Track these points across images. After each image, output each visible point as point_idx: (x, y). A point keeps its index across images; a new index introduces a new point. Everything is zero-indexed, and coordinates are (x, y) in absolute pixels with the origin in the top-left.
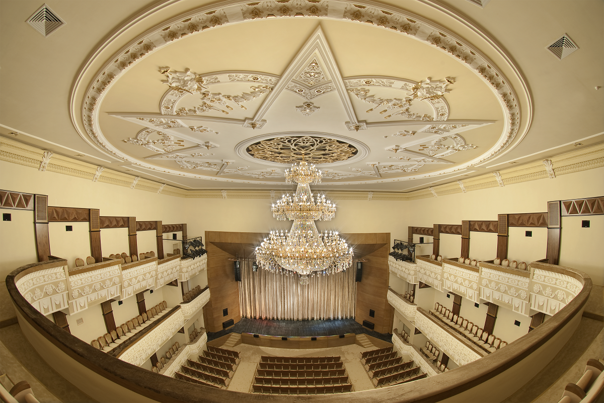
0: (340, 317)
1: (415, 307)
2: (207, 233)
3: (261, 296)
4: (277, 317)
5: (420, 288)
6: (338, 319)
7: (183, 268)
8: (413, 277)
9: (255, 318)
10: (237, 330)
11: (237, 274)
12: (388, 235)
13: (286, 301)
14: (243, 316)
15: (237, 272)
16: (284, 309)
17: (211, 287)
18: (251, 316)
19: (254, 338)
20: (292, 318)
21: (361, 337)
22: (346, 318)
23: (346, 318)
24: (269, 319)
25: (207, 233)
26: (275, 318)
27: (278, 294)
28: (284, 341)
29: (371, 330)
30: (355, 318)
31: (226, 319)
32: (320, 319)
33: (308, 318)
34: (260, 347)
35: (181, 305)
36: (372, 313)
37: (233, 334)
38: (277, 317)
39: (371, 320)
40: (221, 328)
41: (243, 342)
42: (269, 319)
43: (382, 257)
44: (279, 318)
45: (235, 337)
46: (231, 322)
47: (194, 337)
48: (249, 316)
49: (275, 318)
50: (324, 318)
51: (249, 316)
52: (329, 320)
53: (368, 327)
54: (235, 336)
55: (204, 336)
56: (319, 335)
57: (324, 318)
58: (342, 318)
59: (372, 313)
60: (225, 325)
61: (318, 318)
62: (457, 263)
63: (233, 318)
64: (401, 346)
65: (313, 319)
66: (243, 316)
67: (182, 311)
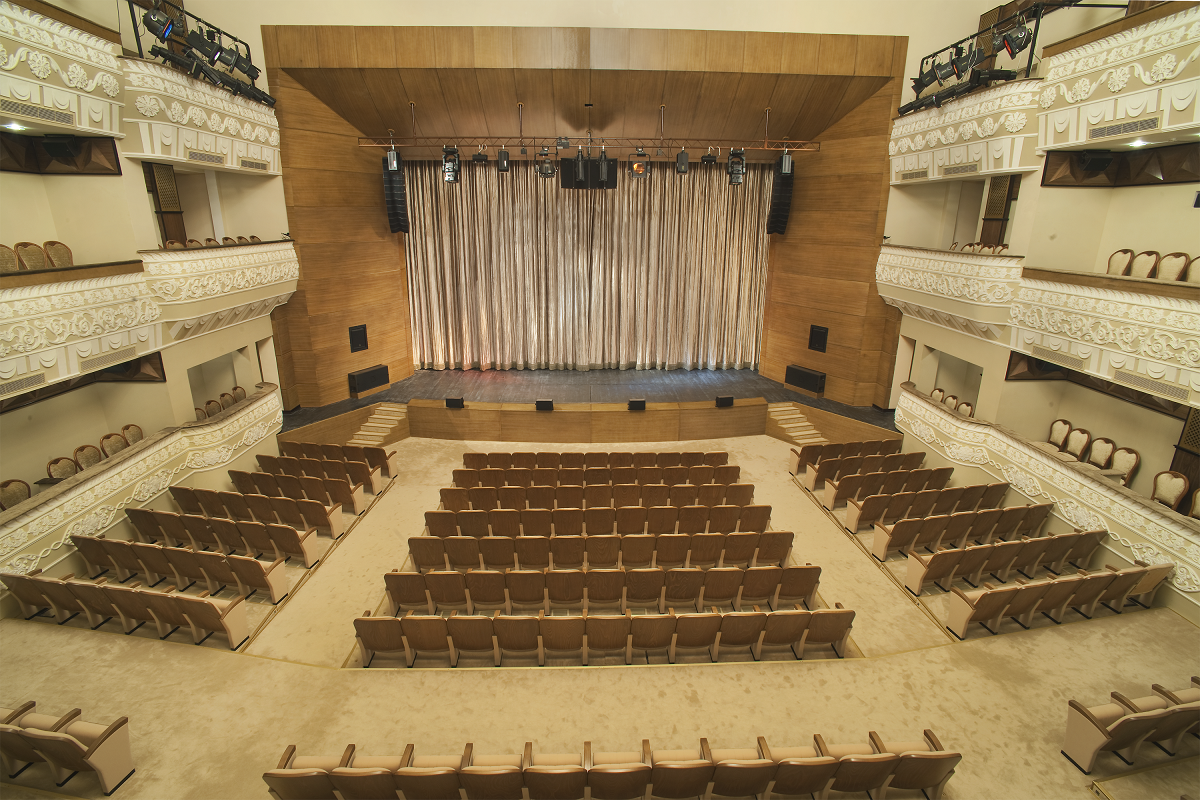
0: (712, 363)
1: (1015, 268)
2: (270, 34)
3: (476, 293)
4: (526, 363)
5: (1044, 184)
6: (705, 368)
7: (142, 93)
8: (1020, 140)
9: (459, 368)
10: (396, 395)
11: (393, 202)
12: (900, 44)
13: (552, 306)
14: (423, 364)
15: (392, 195)
16: (547, 335)
17: (300, 241)
18: (447, 364)
19: (450, 413)
20: (570, 361)
21: (783, 412)
22: (731, 368)
23: (731, 368)
24: (502, 370)
25: (270, 34)
26: (521, 362)
27: (529, 282)
28: (543, 416)
29: (814, 395)
30: (756, 369)
31: (363, 362)
32: (653, 367)
33: (618, 363)
34: (467, 442)
35: (146, 259)
36: (818, 339)
37: (384, 407)
38: (526, 363)
39: (813, 362)
40: (344, 394)
41: (414, 433)
42: (502, 370)
43: (867, 133)
44: (532, 361)
45: (387, 415)
46: (379, 375)
47: (216, 401)
48: (440, 361)
49: (521, 362)
50: (664, 364)
51: (440, 361)
52: (679, 369)
53: (805, 384)
54: (389, 413)
55: (272, 406)
56: (654, 400)
57: (664, 364)
58: (718, 368)
59: (818, 339)
60: (358, 382)
61: (647, 362)
62: (1005, 252)
63: (384, 363)
64: (946, 431)
65: (632, 367)
66: (423, 364)
67: (150, 283)
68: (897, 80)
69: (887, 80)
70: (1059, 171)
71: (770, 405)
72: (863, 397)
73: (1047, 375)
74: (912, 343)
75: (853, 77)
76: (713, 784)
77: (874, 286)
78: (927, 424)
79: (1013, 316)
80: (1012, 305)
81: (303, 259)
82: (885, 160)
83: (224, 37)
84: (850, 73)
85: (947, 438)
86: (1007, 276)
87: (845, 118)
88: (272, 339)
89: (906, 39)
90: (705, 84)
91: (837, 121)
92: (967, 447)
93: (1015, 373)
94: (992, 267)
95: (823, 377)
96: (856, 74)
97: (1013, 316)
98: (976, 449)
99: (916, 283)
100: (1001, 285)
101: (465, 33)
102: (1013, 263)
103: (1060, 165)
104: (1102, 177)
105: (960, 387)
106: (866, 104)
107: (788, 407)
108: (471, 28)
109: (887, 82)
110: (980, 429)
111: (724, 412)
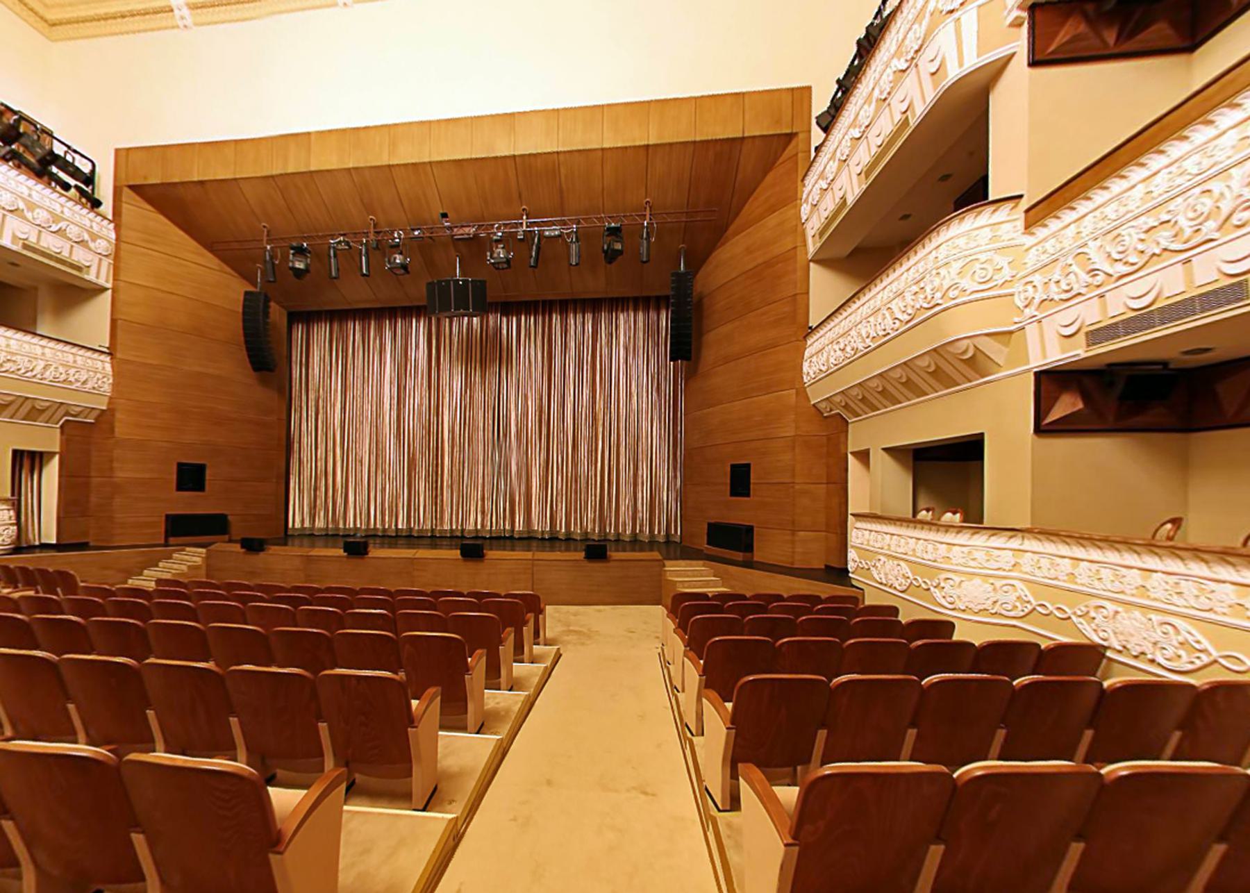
5: (1034, 63)
17: (119, 355)
29: (739, 556)
36: (740, 480)
39: (738, 512)
68: (801, 136)
69: (790, 137)
70: (1062, 33)
71: (667, 563)
72: (812, 551)
73: (1200, 38)
74: (864, 456)
75: (743, 139)
76: (1081, 846)
77: (802, 392)
78: (897, 558)
79: (1021, 305)
80: (1017, 288)
81: (116, 374)
82: (798, 228)
83: (55, 142)
84: (740, 135)
85: (931, 569)
86: (994, 238)
87: (747, 206)
88: (57, 458)
89: (808, 89)
90: (563, 171)
91: (737, 214)
92: (977, 581)
93: (1056, 413)
94: (957, 236)
95: (750, 530)
96: (746, 135)
97: (1021, 305)
98: (999, 583)
99: (848, 349)
100: (983, 257)
101: (302, 139)
102: (1004, 212)
103: (1062, 24)
104: (1160, 30)
105: (948, 473)
106: (769, 178)
107: (277, 307)
108: (309, 134)
109: (790, 141)
110: (999, 541)
111: (597, 566)
